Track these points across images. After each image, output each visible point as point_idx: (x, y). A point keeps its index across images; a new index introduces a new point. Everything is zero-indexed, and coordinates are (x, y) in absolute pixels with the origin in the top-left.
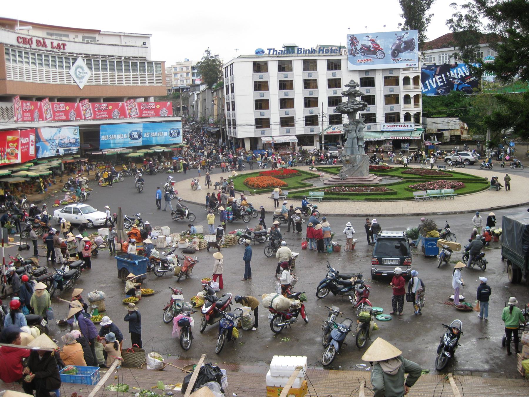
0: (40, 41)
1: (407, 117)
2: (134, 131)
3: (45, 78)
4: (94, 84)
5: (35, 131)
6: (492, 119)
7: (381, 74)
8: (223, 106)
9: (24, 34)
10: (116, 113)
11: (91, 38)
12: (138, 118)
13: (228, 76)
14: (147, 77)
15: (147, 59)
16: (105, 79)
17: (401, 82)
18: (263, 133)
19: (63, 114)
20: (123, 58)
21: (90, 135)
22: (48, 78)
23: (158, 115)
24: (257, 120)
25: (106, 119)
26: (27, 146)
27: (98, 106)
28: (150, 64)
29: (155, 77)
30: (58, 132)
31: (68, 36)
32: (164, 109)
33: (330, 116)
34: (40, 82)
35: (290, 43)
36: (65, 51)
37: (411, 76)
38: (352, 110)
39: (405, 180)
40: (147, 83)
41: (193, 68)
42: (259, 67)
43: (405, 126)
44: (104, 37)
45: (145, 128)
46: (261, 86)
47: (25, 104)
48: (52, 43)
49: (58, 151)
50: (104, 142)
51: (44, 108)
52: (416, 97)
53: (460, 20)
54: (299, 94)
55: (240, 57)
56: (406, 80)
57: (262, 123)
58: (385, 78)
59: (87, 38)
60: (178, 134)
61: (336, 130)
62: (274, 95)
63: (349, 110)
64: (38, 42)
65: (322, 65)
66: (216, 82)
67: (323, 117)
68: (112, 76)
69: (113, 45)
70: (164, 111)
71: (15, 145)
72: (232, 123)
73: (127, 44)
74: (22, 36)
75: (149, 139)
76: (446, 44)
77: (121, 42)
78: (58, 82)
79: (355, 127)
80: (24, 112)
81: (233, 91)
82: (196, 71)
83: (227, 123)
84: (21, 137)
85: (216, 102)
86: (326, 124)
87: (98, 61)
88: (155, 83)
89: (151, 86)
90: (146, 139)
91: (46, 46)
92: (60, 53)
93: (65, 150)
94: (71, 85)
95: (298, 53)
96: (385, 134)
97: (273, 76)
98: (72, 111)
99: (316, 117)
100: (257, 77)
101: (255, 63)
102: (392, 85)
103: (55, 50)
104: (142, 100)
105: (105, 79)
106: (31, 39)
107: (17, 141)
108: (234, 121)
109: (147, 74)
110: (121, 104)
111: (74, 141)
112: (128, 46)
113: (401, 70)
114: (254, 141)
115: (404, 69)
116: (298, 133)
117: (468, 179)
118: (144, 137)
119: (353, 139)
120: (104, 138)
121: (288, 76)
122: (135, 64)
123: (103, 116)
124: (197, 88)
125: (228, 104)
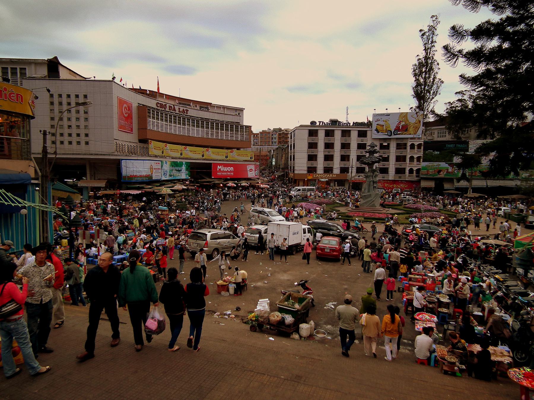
8: (288, 158)
28: (242, 127)
33: (357, 168)
35: (334, 118)
37: (416, 143)
46: (313, 146)
48: (179, 109)
54: (337, 152)
55: (301, 126)
56: (412, 146)
74: (160, 102)
85: (284, 156)
86: (354, 173)
91: (175, 111)
95: (339, 125)
99: (348, 168)
101: (310, 131)
115: (411, 138)
119: (370, 182)
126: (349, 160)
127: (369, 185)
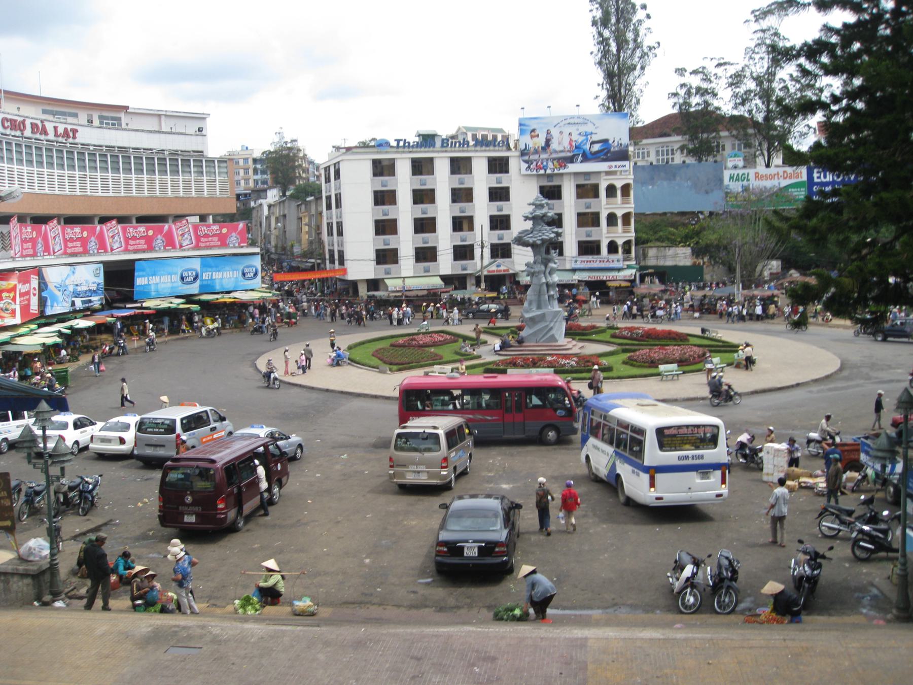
0: (37, 125)
1: (613, 248)
2: (187, 270)
3: (46, 185)
4: (122, 194)
5: (38, 271)
6: (800, 292)
7: (572, 180)
8: (318, 228)
9: (13, 114)
10: (159, 241)
11: (113, 119)
12: (194, 249)
13: (329, 181)
14: (205, 183)
15: (205, 153)
16: (140, 186)
17: (603, 193)
18: (388, 272)
19: (78, 244)
20: (166, 153)
21: (119, 278)
22: (51, 185)
23: (224, 244)
24: (378, 251)
25: (144, 251)
26: (27, 297)
27: (131, 231)
28: (211, 161)
29: (217, 183)
30: (71, 273)
31: (75, 115)
32: (234, 234)
34: (39, 192)
36: (77, 141)
37: (619, 184)
38: (539, 242)
39: (620, 348)
40: (206, 193)
41: (255, 161)
42: (382, 168)
43: (608, 261)
44: (135, 118)
45: (203, 265)
47: (24, 230)
48: (56, 128)
49: (73, 303)
50: (141, 289)
51: (51, 235)
52: (626, 217)
53: (688, 93)
54: (443, 210)
57: (386, 257)
58: (578, 186)
59: (107, 118)
60: (256, 274)
61: (502, 268)
62: (405, 212)
63: (534, 242)
64: (34, 126)
65: (480, 166)
66: (293, 183)
67: (482, 248)
68: (151, 182)
69: (150, 132)
70: (234, 238)
71: (12, 295)
72: (336, 257)
73: (173, 130)
74: (9, 117)
75: (209, 282)
76: (667, 130)
77: (160, 125)
78: (67, 192)
79: (543, 268)
80: (24, 241)
81: (339, 205)
82: (259, 166)
83: (327, 256)
84: (19, 282)
87: (129, 157)
88: (218, 193)
89: (212, 199)
90: (205, 283)
91: (46, 133)
92: (68, 145)
93: (83, 302)
94: (87, 196)
95: (442, 146)
96: (577, 273)
97: (404, 182)
98: (93, 238)
99: (471, 248)
100: (380, 184)
102: (588, 197)
103: (60, 139)
104: (196, 219)
105: (140, 186)
106: (23, 122)
107: (14, 289)
108: (341, 254)
109: (205, 178)
110: (166, 227)
111: (94, 287)
112: (174, 133)
113: (603, 174)
114: (374, 284)
116: (442, 273)
117: (712, 346)
118: (202, 280)
120: (140, 281)
121: (427, 182)
122: (186, 162)
123: (140, 247)
124: (262, 194)
125: (330, 225)
126: (471, 228)
127: (540, 294)
